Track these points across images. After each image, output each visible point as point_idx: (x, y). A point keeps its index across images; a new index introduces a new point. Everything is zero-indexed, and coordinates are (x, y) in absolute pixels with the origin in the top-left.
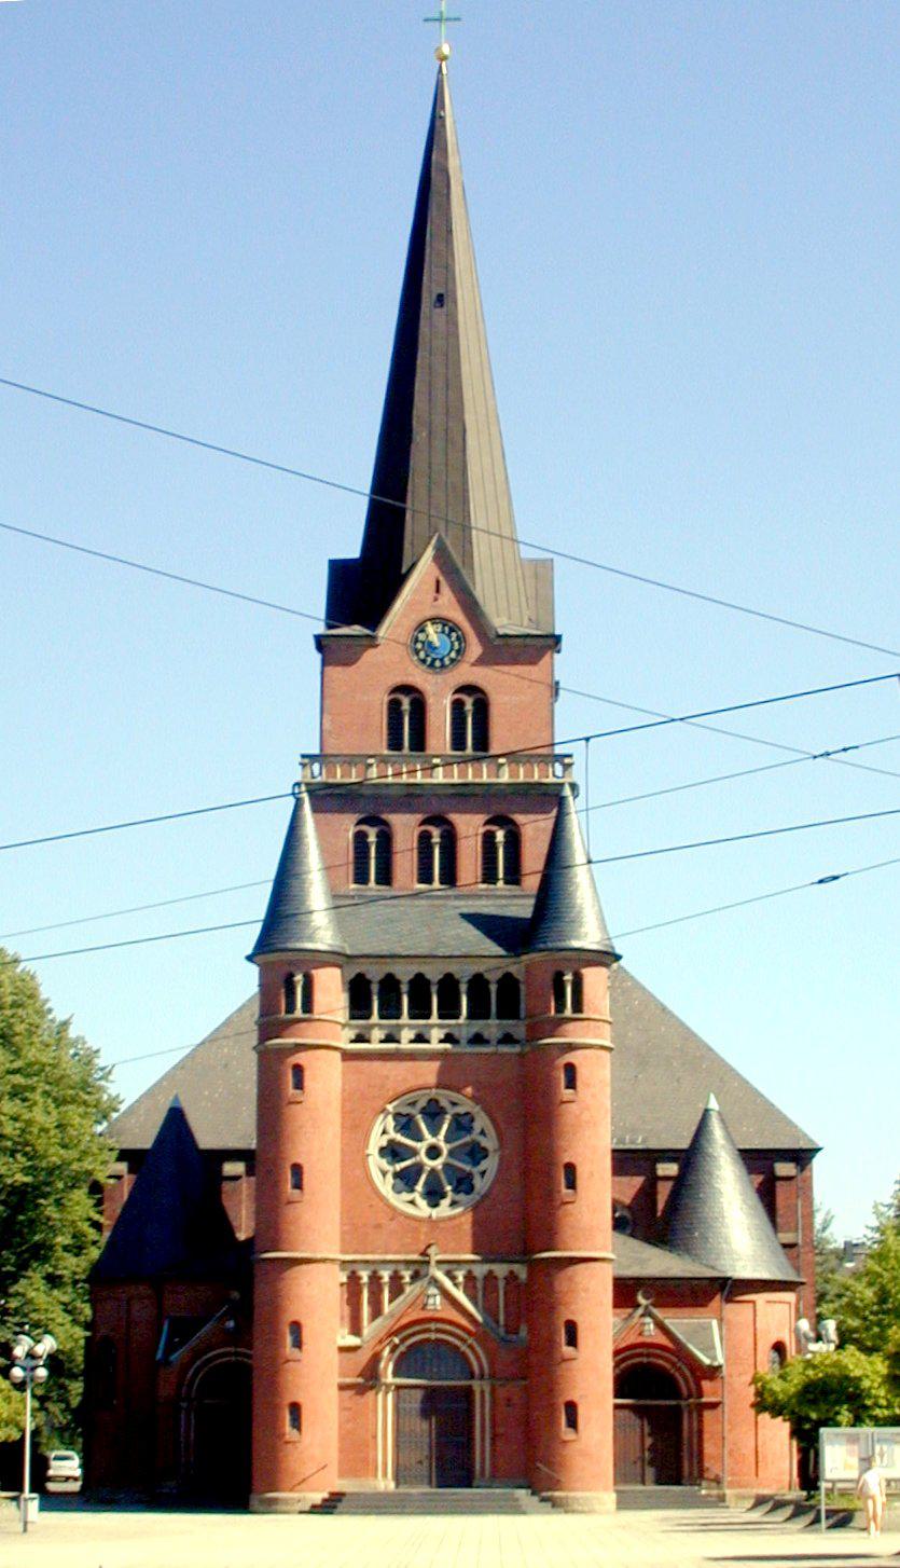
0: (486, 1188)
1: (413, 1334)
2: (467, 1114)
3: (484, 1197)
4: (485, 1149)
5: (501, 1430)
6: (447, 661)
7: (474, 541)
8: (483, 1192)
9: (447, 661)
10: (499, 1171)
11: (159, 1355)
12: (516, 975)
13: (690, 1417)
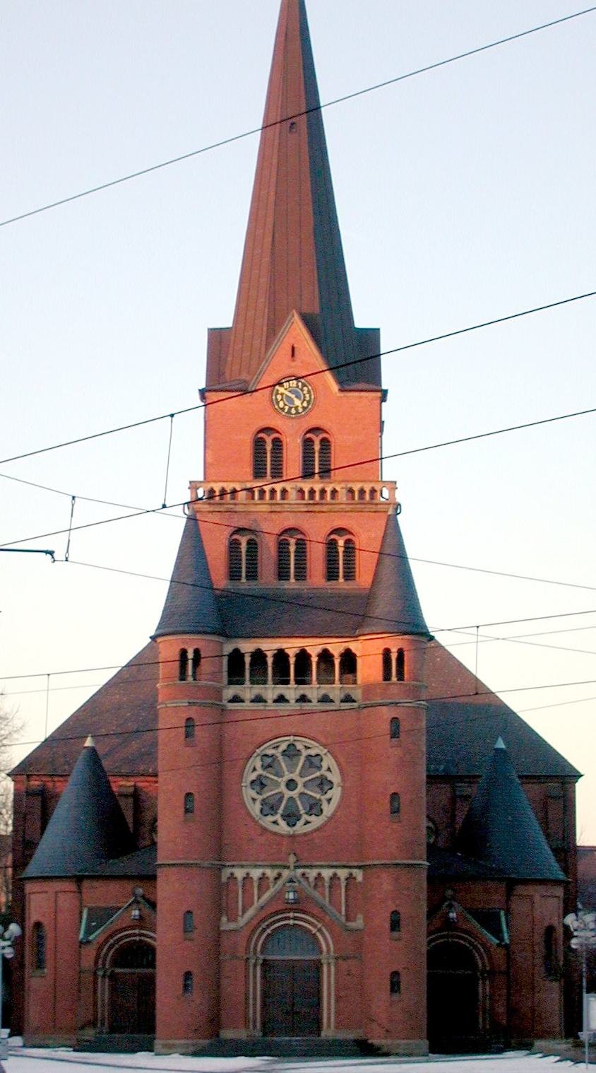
0: (300, 832)
1: (257, 941)
2: (317, 755)
3: (330, 819)
4: (331, 782)
5: (342, 994)
6: (300, 410)
7: (317, 300)
8: (329, 815)
9: (300, 410)
10: (342, 798)
11: (81, 936)
12: (353, 651)
13: (484, 983)
